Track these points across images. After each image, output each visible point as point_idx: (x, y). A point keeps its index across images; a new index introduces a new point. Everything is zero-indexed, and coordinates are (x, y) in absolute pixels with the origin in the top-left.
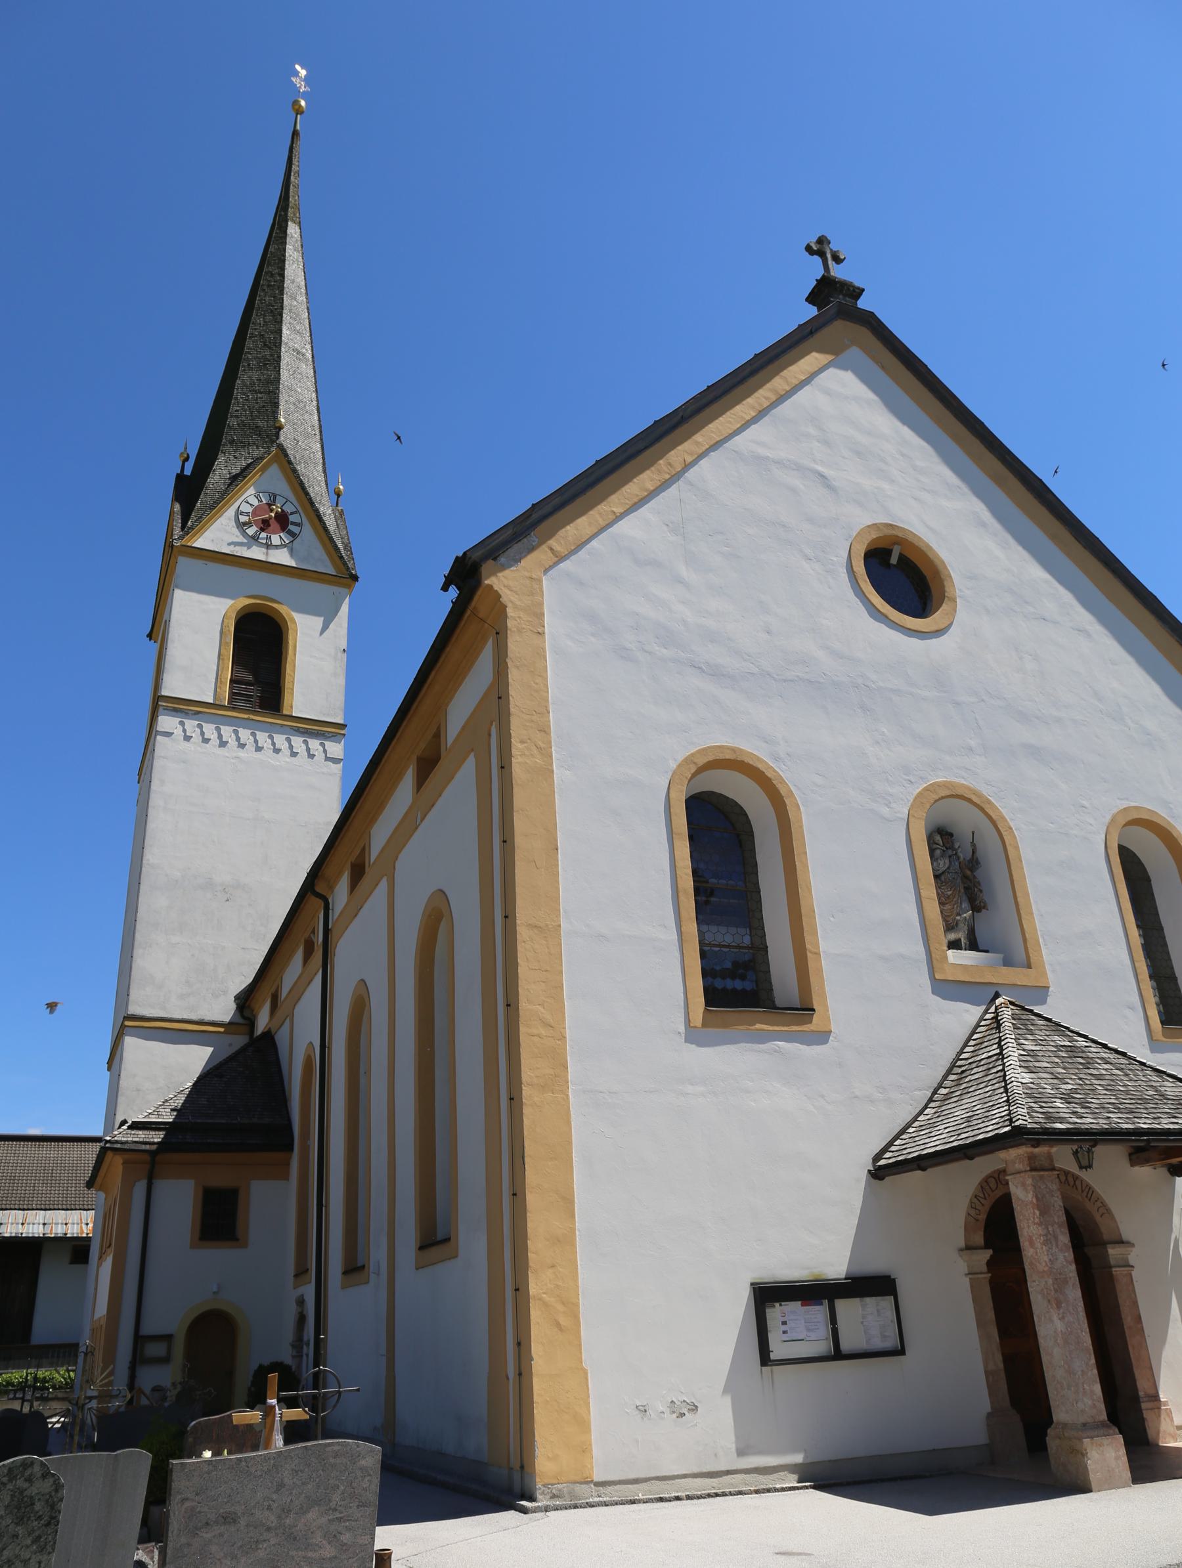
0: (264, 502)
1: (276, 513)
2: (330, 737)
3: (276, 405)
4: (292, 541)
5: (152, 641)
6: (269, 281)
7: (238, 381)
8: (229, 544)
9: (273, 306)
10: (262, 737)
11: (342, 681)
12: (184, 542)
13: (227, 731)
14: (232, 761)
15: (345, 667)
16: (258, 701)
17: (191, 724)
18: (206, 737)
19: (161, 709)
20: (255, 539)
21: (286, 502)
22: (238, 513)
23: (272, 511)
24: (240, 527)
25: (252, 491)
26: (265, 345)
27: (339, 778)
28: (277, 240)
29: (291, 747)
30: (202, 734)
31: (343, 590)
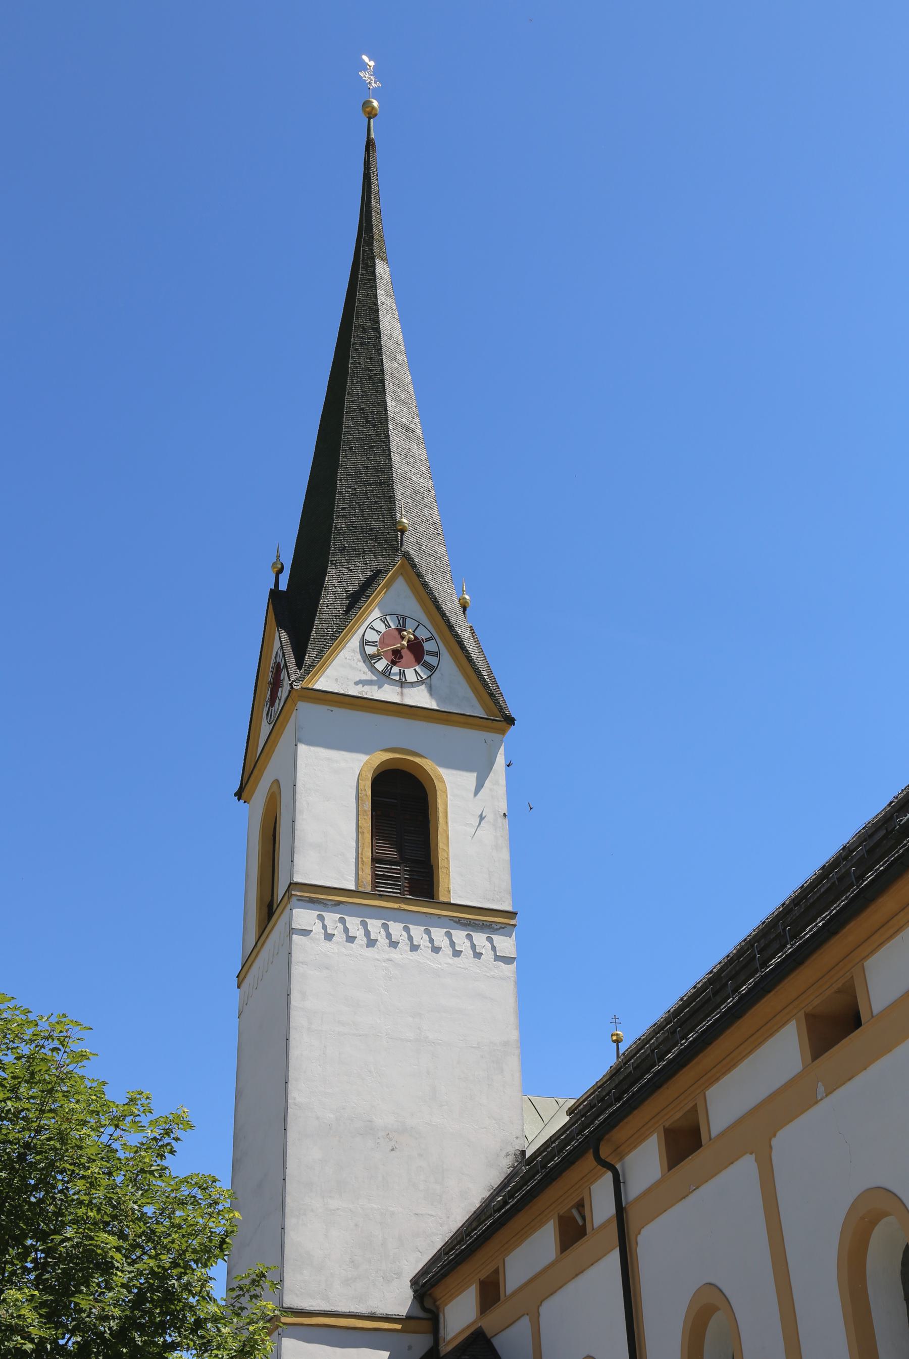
0: (393, 627)
1: (409, 641)
2: (497, 929)
3: (391, 500)
4: (430, 676)
5: (242, 801)
6: (362, 338)
7: (340, 471)
8: (357, 683)
9: (371, 371)
10: (417, 932)
11: (505, 855)
12: (304, 684)
13: (375, 926)
14: (384, 964)
15: (507, 837)
16: (406, 885)
17: (331, 918)
18: (350, 934)
19: (294, 899)
20: (386, 674)
21: (419, 625)
22: (364, 643)
23: (403, 638)
24: (367, 661)
25: (376, 613)
26: (367, 422)
27: (513, 983)
28: (365, 284)
29: (452, 944)
30: (346, 930)
31: (496, 736)
